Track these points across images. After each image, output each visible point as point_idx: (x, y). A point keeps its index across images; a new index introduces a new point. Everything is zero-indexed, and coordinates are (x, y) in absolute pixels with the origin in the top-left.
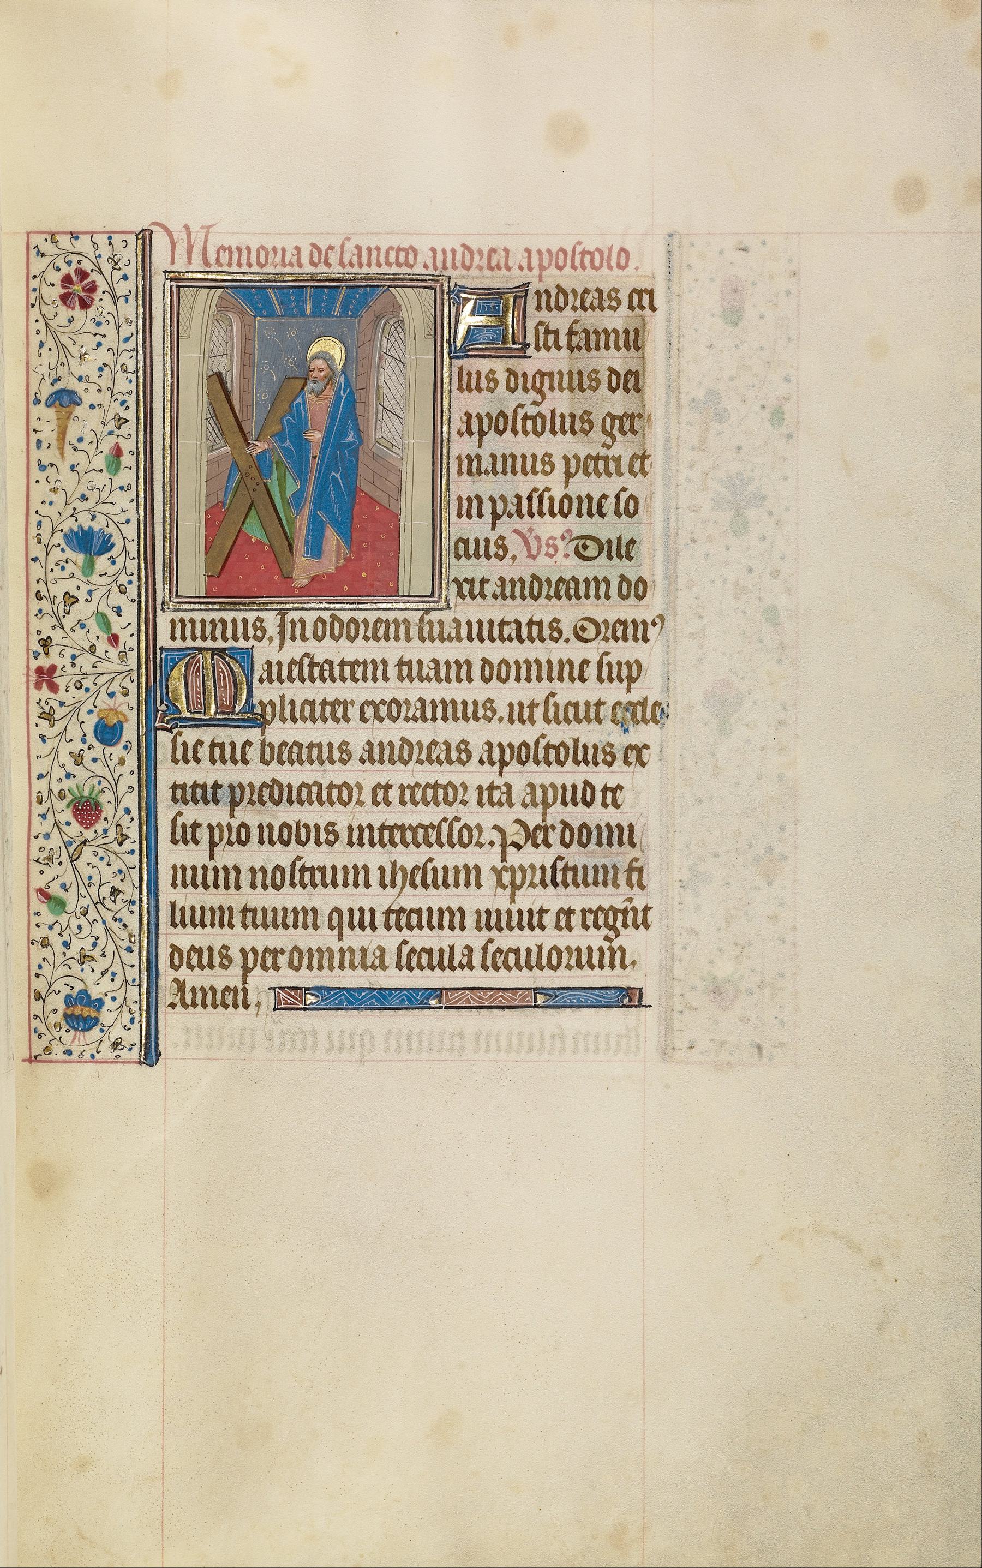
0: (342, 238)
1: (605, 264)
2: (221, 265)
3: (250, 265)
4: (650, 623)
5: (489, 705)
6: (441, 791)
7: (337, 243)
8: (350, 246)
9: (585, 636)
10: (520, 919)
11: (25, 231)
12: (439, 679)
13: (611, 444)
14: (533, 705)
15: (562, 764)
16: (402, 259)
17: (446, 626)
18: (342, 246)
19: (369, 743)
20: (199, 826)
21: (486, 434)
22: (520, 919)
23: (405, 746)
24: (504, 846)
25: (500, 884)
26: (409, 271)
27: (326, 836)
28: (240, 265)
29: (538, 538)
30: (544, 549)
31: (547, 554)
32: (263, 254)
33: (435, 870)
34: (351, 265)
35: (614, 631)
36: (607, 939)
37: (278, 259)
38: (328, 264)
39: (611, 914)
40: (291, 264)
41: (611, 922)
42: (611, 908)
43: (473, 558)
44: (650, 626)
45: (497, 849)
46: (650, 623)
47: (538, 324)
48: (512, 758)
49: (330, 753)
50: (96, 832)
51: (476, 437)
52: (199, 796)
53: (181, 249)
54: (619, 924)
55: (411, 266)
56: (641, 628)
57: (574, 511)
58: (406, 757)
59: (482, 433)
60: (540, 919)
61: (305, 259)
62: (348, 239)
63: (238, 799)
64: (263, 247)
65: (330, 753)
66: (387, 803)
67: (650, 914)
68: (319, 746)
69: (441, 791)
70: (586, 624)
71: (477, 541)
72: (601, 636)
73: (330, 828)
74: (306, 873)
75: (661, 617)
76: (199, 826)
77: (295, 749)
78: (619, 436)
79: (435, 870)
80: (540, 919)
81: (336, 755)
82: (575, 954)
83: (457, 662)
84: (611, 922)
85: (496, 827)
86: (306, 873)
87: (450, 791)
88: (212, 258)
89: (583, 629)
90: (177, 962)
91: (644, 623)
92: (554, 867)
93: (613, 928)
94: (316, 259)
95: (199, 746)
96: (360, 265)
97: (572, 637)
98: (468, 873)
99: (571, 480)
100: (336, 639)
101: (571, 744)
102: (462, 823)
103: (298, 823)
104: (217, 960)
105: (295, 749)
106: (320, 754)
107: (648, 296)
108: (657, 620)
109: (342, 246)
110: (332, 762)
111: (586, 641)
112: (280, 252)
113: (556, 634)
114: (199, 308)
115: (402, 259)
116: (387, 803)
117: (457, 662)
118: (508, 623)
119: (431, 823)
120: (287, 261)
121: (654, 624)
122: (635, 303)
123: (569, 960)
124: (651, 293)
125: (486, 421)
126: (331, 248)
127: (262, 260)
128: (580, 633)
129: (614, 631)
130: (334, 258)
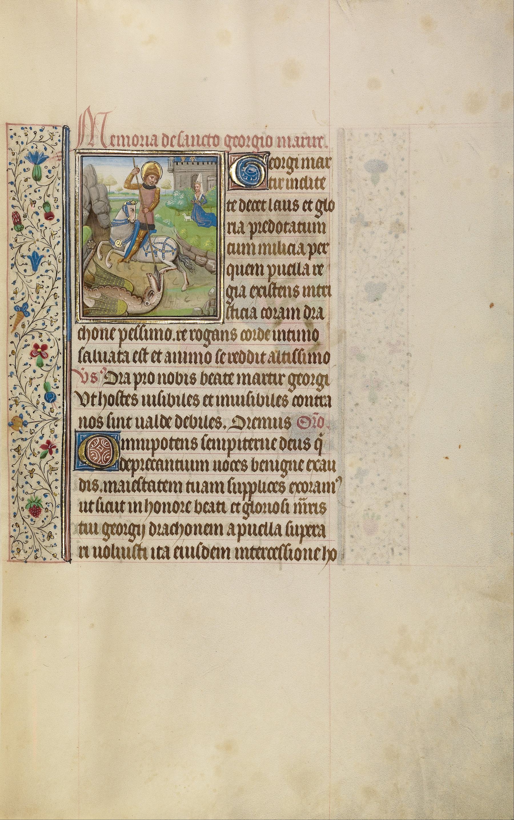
2: (113, 146)
3: (129, 145)
8: (183, 135)
10: (238, 400)
12: (140, 558)
13: (293, 390)
18: (179, 136)
20: (124, 503)
22: (238, 400)
23: (152, 527)
27: (282, 402)
28: (124, 145)
29: (86, 374)
32: (135, 139)
35: (147, 465)
36: (288, 173)
37: (144, 143)
38: (172, 145)
40: (152, 145)
43: (209, 428)
51: (151, 451)
52: (179, 467)
57: (193, 532)
58: (269, 315)
59: (154, 449)
60: (280, 379)
61: (160, 142)
62: (182, 132)
63: (138, 381)
64: (135, 136)
68: (182, 462)
69: (211, 140)
70: (305, 420)
71: (309, 224)
76: (124, 503)
77: (160, 463)
78: (297, 386)
80: (280, 379)
88: (107, 141)
89: (302, 422)
94: (165, 143)
95: (275, 441)
96: (156, 145)
99: (231, 452)
102: (222, 352)
104: (292, 207)
105: (160, 463)
109: (179, 136)
112: (145, 139)
123: (249, 425)
124: (329, 288)
126: (174, 137)
127: (135, 143)
129: (147, 465)
130: (175, 142)
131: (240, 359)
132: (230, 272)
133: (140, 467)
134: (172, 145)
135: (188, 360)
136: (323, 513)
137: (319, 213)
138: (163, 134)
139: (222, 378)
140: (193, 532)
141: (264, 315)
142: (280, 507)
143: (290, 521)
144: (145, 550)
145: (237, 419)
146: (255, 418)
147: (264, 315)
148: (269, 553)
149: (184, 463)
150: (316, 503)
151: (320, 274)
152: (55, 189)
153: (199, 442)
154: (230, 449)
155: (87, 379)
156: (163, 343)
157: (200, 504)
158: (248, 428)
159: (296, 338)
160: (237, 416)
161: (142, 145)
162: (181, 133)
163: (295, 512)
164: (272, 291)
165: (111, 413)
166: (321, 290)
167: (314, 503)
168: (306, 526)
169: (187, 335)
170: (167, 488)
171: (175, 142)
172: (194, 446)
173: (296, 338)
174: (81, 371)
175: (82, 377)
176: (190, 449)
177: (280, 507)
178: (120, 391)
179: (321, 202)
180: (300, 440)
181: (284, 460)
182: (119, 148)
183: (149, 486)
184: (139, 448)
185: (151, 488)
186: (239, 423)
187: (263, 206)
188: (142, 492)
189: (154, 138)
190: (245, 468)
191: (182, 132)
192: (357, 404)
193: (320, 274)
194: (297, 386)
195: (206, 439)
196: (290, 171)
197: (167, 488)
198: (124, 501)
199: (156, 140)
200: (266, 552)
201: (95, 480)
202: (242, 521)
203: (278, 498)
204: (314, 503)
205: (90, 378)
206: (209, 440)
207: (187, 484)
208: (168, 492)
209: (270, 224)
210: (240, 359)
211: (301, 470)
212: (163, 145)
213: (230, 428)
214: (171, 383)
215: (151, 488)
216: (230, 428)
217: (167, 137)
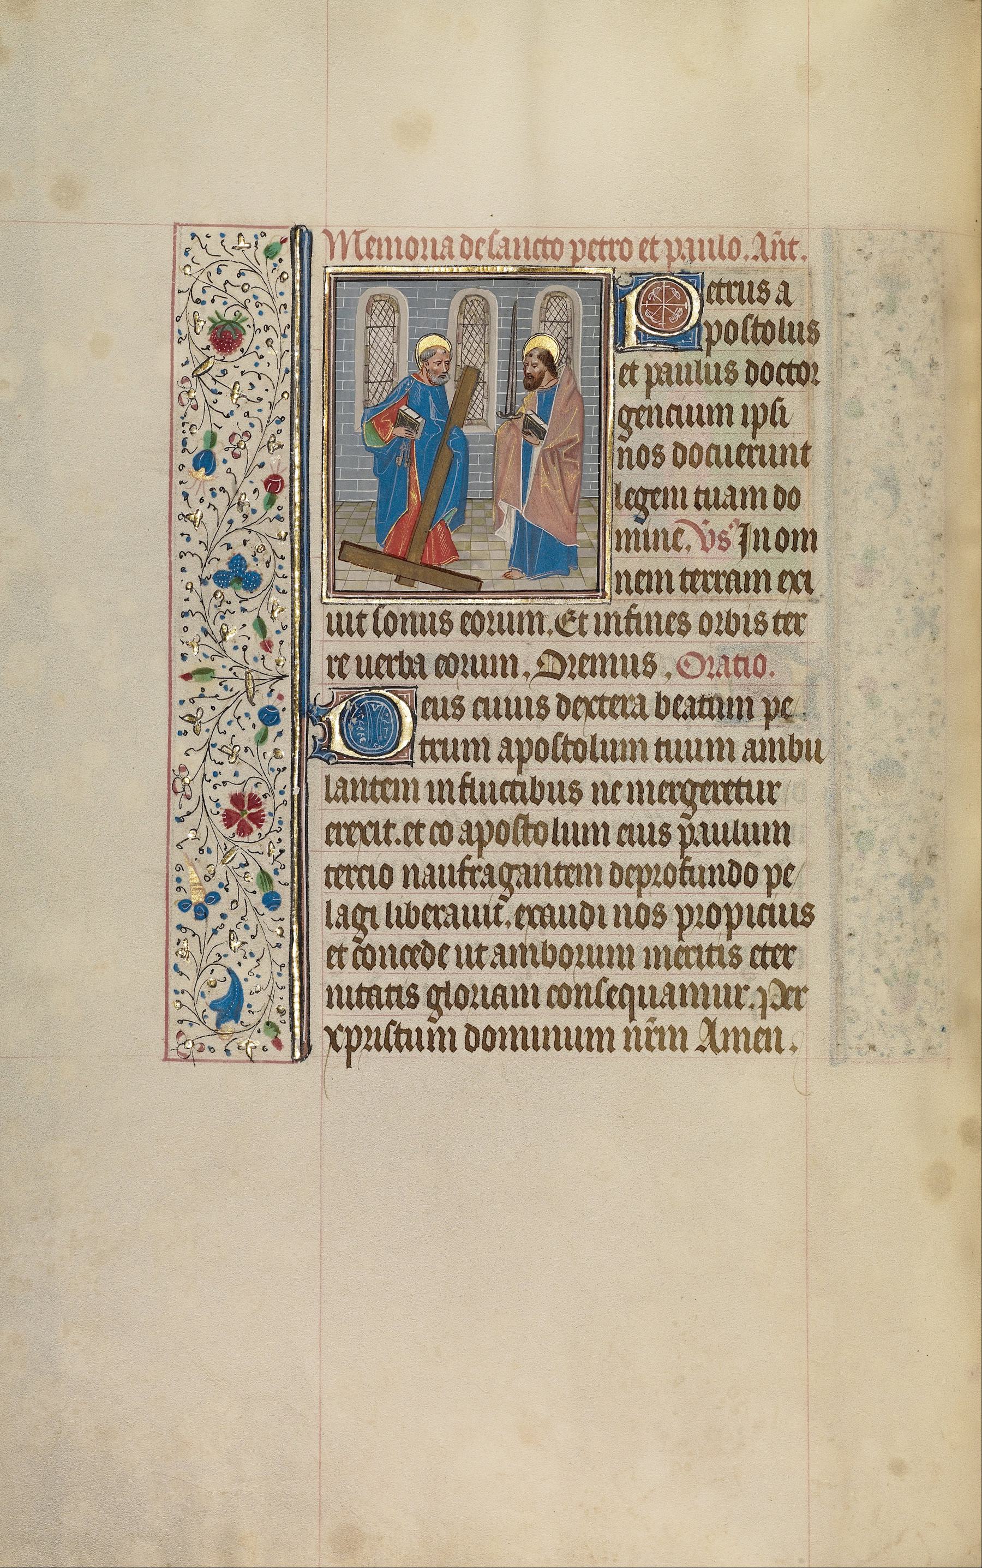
0: (492, 230)
1: (588, 755)
6: (794, 371)
7: (486, 237)
8: (498, 239)
9: (688, 671)
11: (293, 225)
14: (362, 616)
15: (390, 634)
16: (549, 252)
17: (722, 493)
18: (491, 238)
21: (715, 343)
24: (764, 1006)
25: (334, 1046)
26: (555, 263)
29: (711, 532)
30: (717, 543)
31: (720, 547)
32: (412, 245)
35: (582, 666)
36: (638, 520)
37: (429, 252)
38: (479, 256)
39: (689, 788)
41: (688, 796)
42: (689, 781)
47: (747, 317)
49: (751, 291)
50: (282, 558)
55: (557, 258)
57: (378, 962)
61: (456, 251)
65: (751, 291)
67: (484, 954)
69: (794, 371)
70: (690, 658)
73: (574, 787)
74: (402, 1035)
77: (733, 577)
82: (470, 662)
83: (756, 572)
84: (688, 796)
86: (402, 1035)
87: (803, 370)
89: (687, 664)
93: (691, 803)
103: (736, 823)
106: (668, 752)
109: (491, 238)
111: (688, 677)
114: (351, 575)
115: (549, 252)
117: (756, 572)
119: (778, 944)
120: (438, 253)
122: (437, 837)
125: (526, 747)
127: (412, 252)
128: (685, 669)
129: (582, 666)
130: (484, 250)
132: (413, 913)
134: (479, 256)
135: (515, 627)
136: (807, 925)
138: (463, 236)
139: (553, 874)
140: (378, 962)
141: (360, 962)
142: (589, 749)
143: (778, 398)
145: (548, 660)
146: (584, 656)
147: (360, 962)
152: (236, 664)
157: (416, 909)
158: (572, 676)
160: (548, 652)
161: (424, 257)
162: (495, 236)
163: (627, 1048)
165: (780, 399)
168: (789, 1008)
170: (390, 791)
171: (484, 250)
174: (702, 527)
176: (439, 634)
177: (589, 749)
180: (751, 284)
181: (359, 906)
182: (389, 263)
184: (807, 549)
186: (552, 665)
189: (447, 243)
191: (496, 232)
197: (390, 791)
198: (585, 613)
199: (451, 247)
200: (617, 249)
202: (633, 526)
203: (729, 977)
208: (392, 802)
209: (425, 949)
211: (616, 802)
212: (462, 254)
213: (536, 676)
214: (795, 760)
216: (536, 676)
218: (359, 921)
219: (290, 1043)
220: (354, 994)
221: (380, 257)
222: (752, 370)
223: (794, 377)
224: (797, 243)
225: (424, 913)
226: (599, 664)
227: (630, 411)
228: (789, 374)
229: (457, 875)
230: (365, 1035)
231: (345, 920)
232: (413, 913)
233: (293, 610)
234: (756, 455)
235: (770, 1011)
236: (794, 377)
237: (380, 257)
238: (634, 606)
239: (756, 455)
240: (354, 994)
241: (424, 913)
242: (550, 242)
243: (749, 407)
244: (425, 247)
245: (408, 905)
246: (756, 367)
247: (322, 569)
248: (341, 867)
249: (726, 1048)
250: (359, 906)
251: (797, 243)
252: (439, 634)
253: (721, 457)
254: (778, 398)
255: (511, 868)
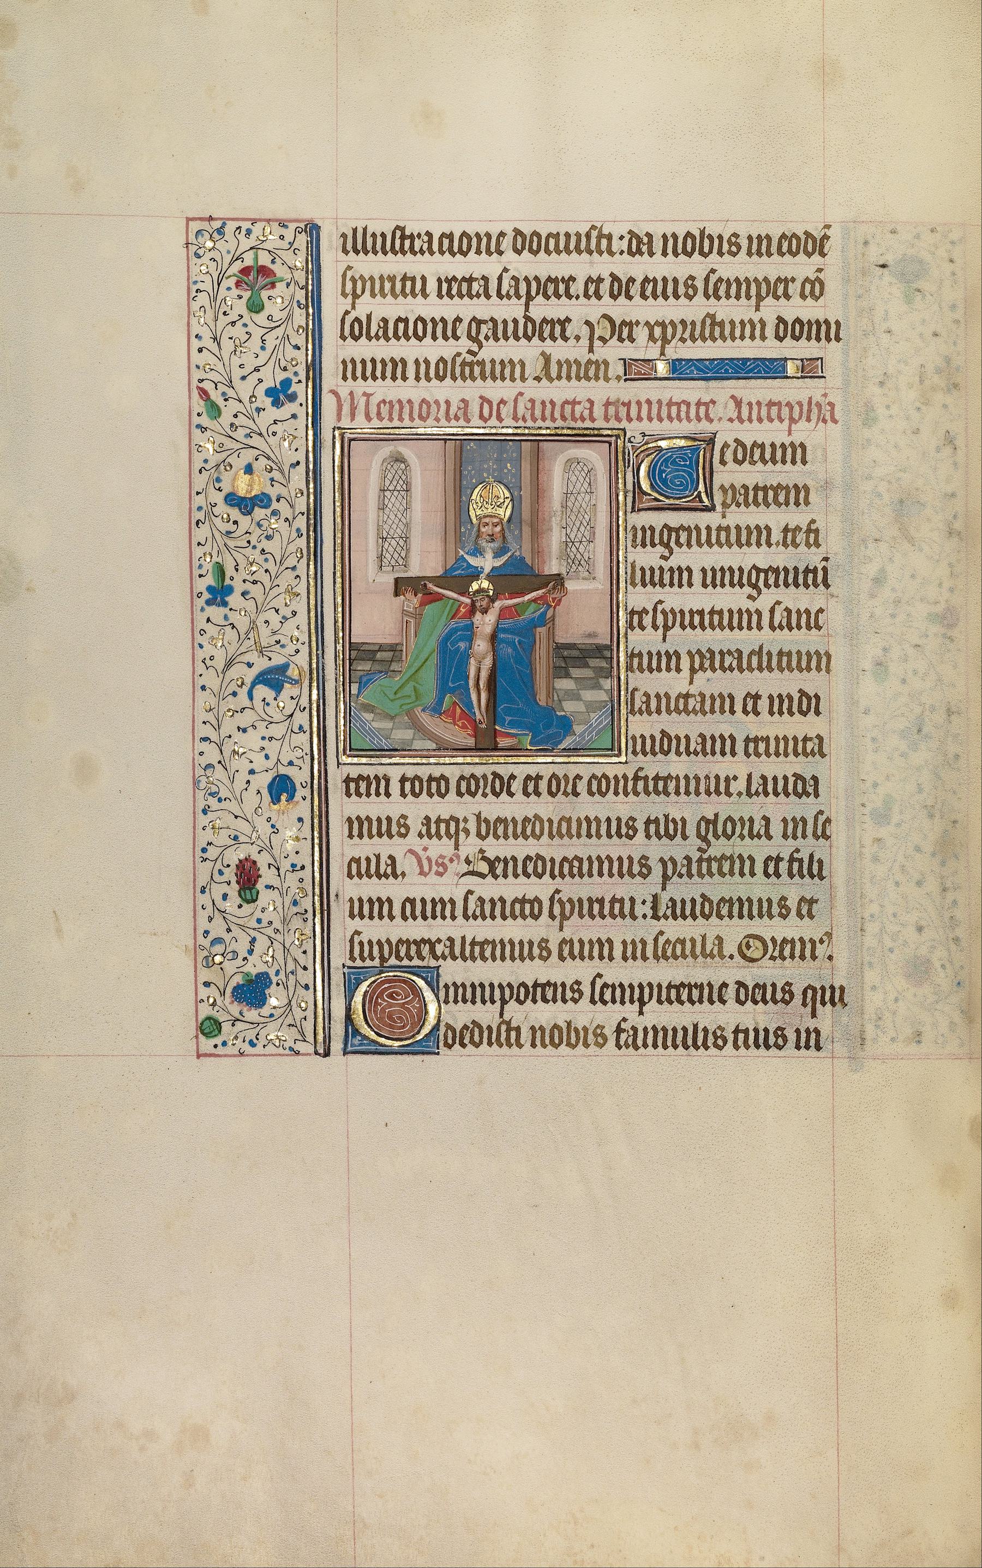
4: (817, 941)
5: (780, 1033)
6: (527, 906)
9: (748, 954)
18: (516, 400)
19: (427, 819)
25: (651, 337)
33: (361, 943)
34: (583, 419)
35: (782, 951)
44: (818, 945)
45: (585, 342)
46: (817, 941)
48: (511, 998)
51: (661, 631)
53: (346, 409)
54: (761, 584)
56: (809, 946)
61: (598, 411)
66: (537, 793)
69: (527, 906)
72: (768, 956)
75: (827, 934)
78: (764, 590)
79: (361, 943)
81: (636, 869)
85: (587, 323)
89: (748, 947)
90: (742, 997)
91: (812, 941)
92: (454, 360)
93: (755, 586)
97: (736, 954)
98: (570, 367)
100: (536, 234)
101: (564, 1026)
107: (759, 450)
108: (825, 938)
109: (516, 400)
110: (632, 875)
111: (753, 960)
113: (718, 952)
116: (537, 793)
118: (811, 739)
121: (822, 941)
126: (502, 402)
129: (782, 951)
131: (533, 830)
133: (678, 336)
137: (704, 844)
140: (485, 1040)
143: (598, 974)
144: (721, 324)
148: (674, 947)
149: (726, 616)
150: (768, 737)
151: (811, 916)
153: (700, 284)
154: (666, 628)
155: (430, 870)
156: (480, 303)
159: (574, 831)
164: (398, 242)
166: (761, 494)
167: (597, 898)
169: (763, 705)
172: (780, 1041)
173: (574, 831)
174: (421, 853)
175: (421, 866)
178: (708, 315)
179: (708, 822)
181: (754, 567)
183: (571, 867)
185: (575, 870)
187: (755, 704)
188: (370, 254)
190: (788, 988)
192: (955, 822)
193: (811, 916)
194: (764, 590)
195: (713, 279)
196: (754, 593)
201: (788, 984)
204: (597, 898)
205: (434, 868)
206: (720, 280)
207: (696, 404)
210: (533, 830)
215: (575, 870)
217: (490, 403)
218: (754, 581)
219: (682, 513)
220: (714, 534)
221: (544, 419)
222: (782, 326)
223: (527, 912)
224: (816, 901)
225: (541, 327)
226: (736, 907)
227: (758, 570)
228: (522, 910)
229: (630, 784)
230: (680, 328)
231: (674, 912)
232: (573, 1034)
233: (308, 598)
234: (477, 370)
235: (597, 343)
236: (527, 912)
237: (544, 419)
238: (797, 851)
239: (477, 370)
240: (714, 534)
241: (541, 327)
242: (637, 612)
243: (778, 446)
244: (552, 413)
245: (666, 817)
246: (785, 323)
247: (335, 582)
248: (576, 858)
249: (559, 377)
250: (754, 567)
251: (816, 901)
252: (537, 959)
253: (731, 539)
254: (598, 974)
255: (479, 322)
